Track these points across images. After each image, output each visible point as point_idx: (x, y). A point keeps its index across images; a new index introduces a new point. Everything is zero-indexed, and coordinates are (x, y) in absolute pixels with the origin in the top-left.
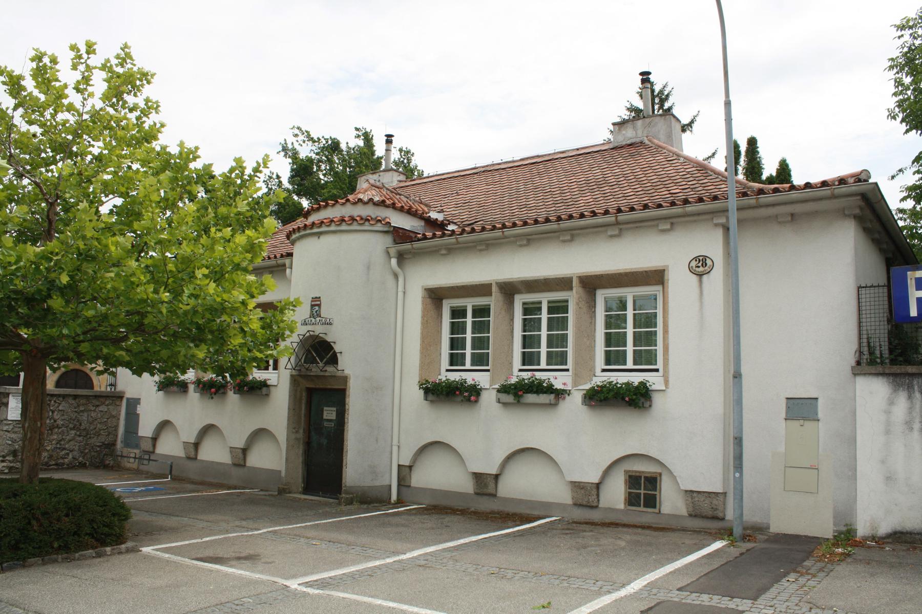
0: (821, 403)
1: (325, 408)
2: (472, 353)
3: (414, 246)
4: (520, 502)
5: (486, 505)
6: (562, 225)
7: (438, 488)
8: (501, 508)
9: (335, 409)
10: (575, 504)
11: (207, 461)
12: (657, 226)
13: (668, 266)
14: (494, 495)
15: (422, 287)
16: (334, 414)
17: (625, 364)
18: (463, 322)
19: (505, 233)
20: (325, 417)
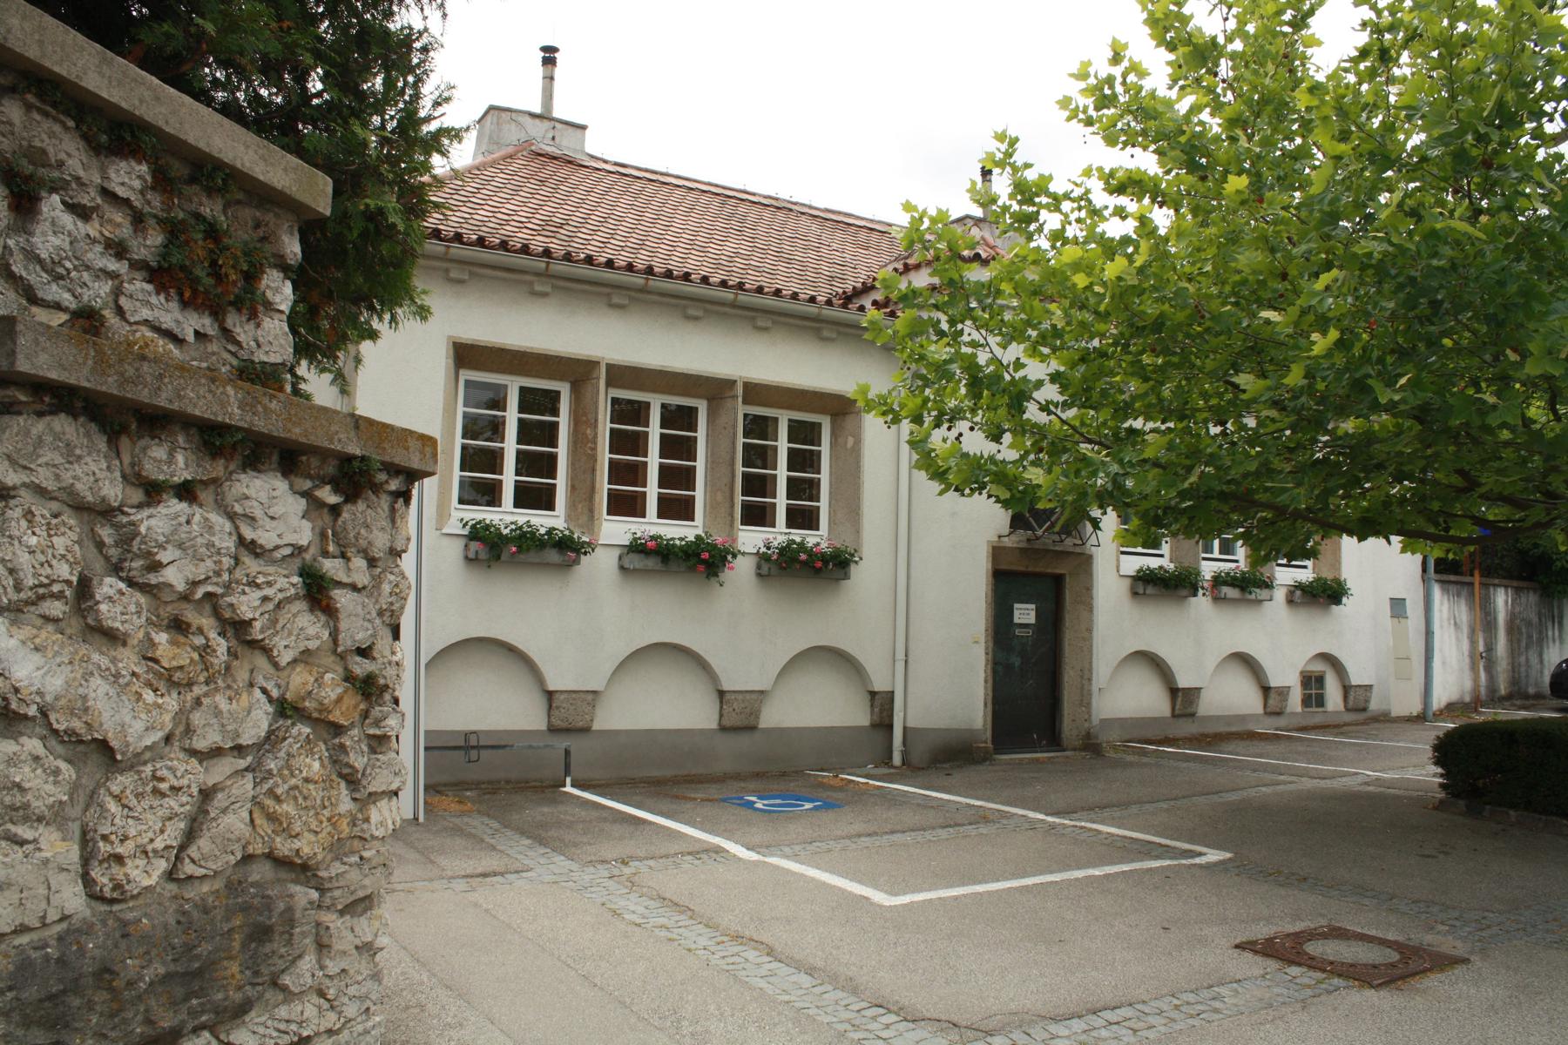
0: (1408, 602)
1: (1016, 606)
2: (554, 478)
3: (651, 283)
4: (1218, 718)
5: (1187, 728)
6: (740, 297)
7: (1127, 715)
8: (1201, 730)
9: (1033, 606)
10: (723, 729)
11: (627, 732)
12: (685, 307)
13: (449, 337)
14: (1193, 715)
15: (449, 337)
16: (1033, 614)
17: (1212, 553)
18: (689, 438)
19: (452, 251)
20: (1016, 620)
